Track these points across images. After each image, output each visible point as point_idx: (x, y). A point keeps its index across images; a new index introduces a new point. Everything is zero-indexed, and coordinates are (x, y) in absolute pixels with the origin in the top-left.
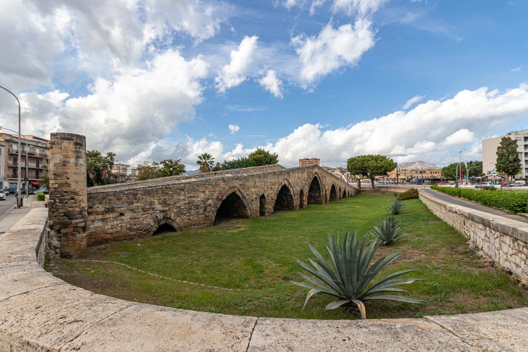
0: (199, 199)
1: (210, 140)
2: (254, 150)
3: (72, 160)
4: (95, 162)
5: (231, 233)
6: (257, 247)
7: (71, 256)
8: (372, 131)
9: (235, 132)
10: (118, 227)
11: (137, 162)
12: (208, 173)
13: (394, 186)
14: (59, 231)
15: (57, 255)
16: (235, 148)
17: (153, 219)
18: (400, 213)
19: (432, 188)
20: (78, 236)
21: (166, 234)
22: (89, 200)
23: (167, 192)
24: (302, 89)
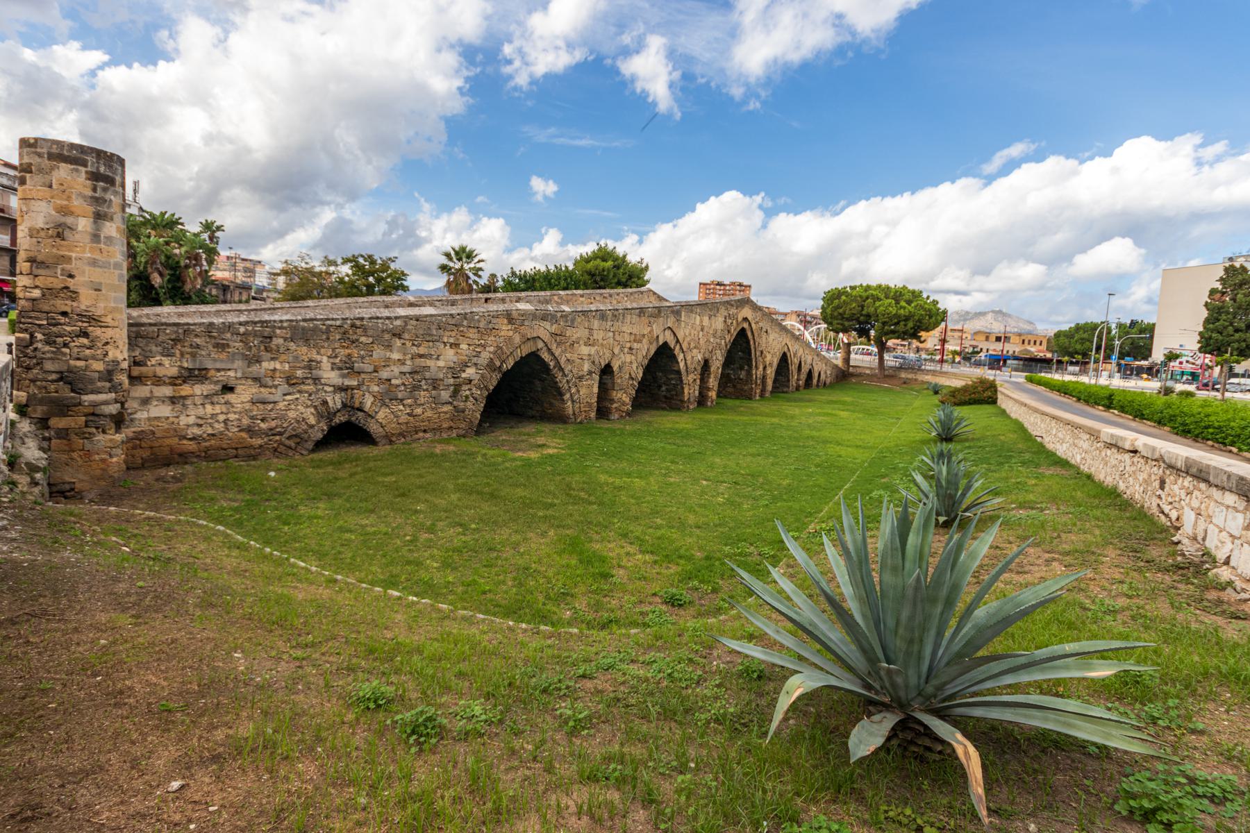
0: (441, 363)
1: (477, 213)
2: (589, 248)
3: (84, 224)
4: (167, 243)
5: (521, 459)
6: (591, 503)
7: (80, 492)
8: (893, 224)
9: (546, 197)
10: (218, 421)
11: (281, 254)
12: (467, 296)
13: (932, 368)
14: (43, 423)
15: (36, 490)
16: (541, 239)
17: (315, 407)
18: (954, 439)
19: (1030, 380)
20: (99, 441)
21: (347, 449)
22: (132, 344)
23: (355, 337)
24: (732, 99)
